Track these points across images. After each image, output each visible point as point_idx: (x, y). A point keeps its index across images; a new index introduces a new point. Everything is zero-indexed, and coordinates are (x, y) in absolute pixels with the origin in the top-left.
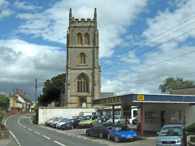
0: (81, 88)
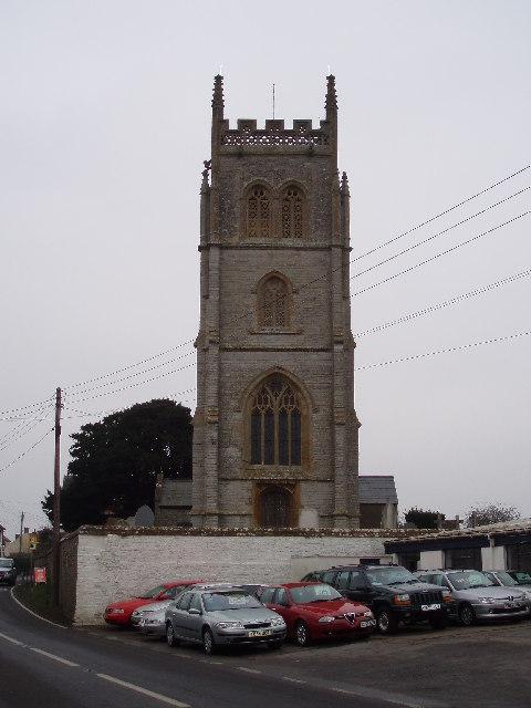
0: (269, 441)
